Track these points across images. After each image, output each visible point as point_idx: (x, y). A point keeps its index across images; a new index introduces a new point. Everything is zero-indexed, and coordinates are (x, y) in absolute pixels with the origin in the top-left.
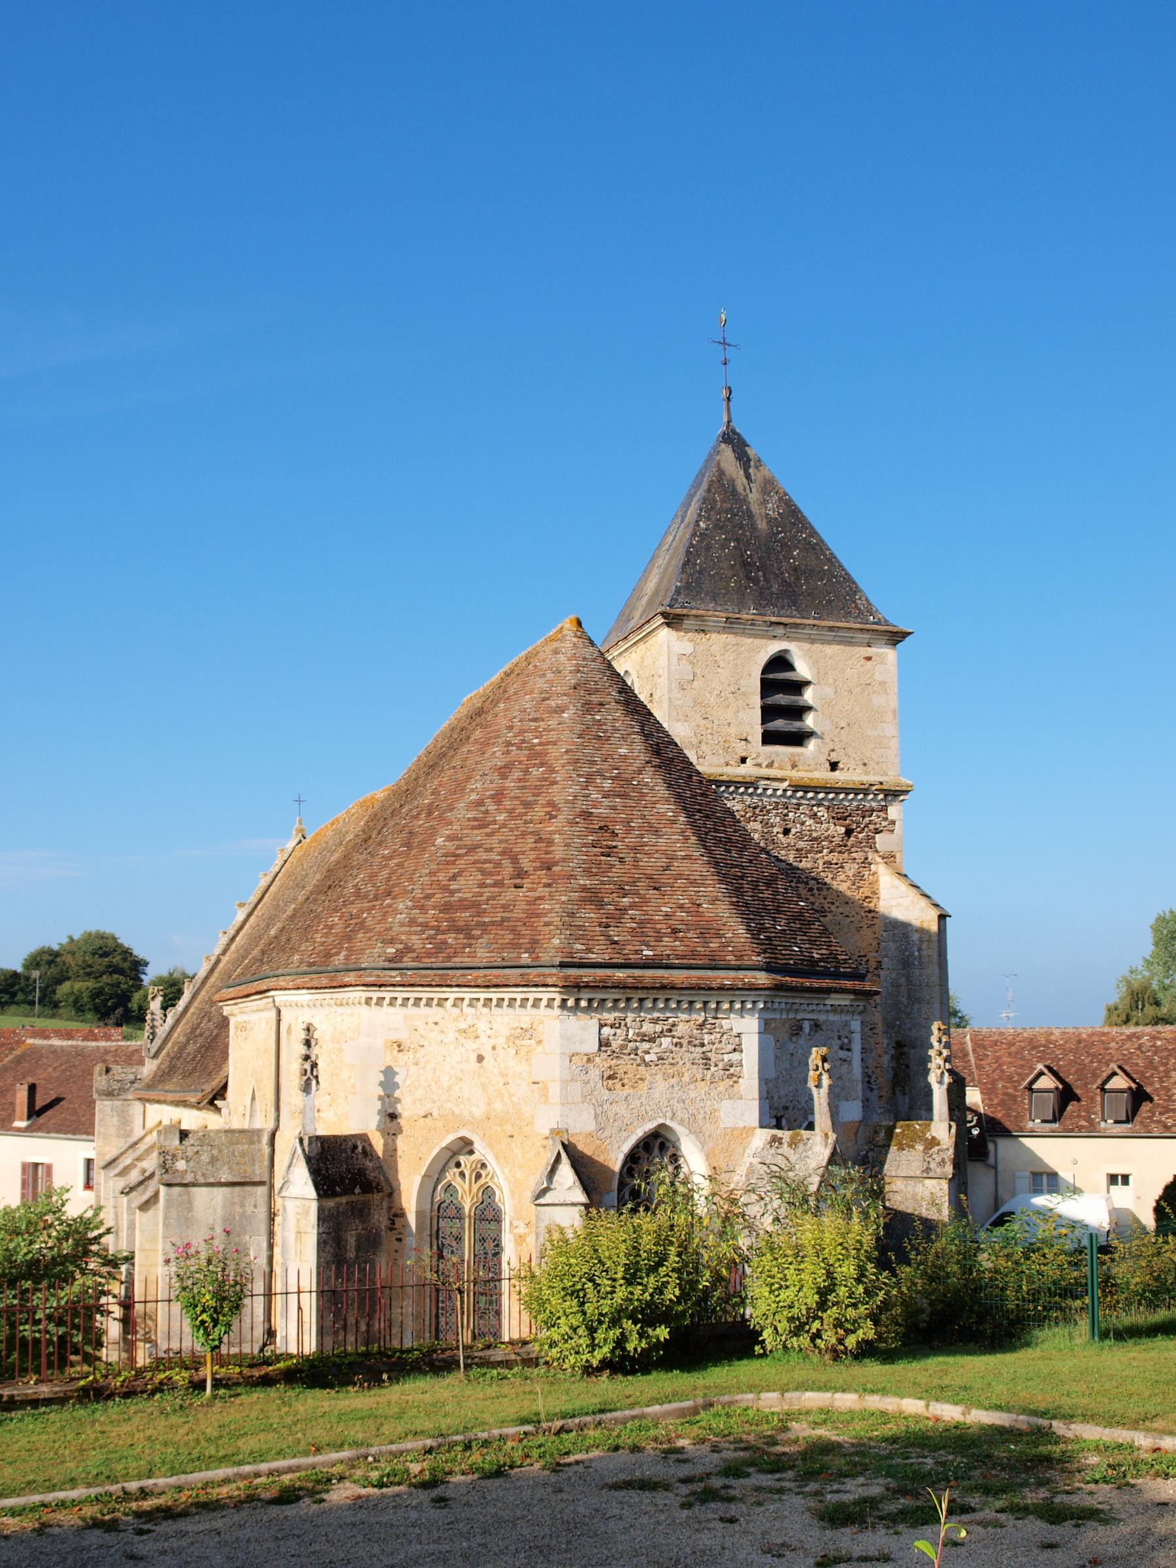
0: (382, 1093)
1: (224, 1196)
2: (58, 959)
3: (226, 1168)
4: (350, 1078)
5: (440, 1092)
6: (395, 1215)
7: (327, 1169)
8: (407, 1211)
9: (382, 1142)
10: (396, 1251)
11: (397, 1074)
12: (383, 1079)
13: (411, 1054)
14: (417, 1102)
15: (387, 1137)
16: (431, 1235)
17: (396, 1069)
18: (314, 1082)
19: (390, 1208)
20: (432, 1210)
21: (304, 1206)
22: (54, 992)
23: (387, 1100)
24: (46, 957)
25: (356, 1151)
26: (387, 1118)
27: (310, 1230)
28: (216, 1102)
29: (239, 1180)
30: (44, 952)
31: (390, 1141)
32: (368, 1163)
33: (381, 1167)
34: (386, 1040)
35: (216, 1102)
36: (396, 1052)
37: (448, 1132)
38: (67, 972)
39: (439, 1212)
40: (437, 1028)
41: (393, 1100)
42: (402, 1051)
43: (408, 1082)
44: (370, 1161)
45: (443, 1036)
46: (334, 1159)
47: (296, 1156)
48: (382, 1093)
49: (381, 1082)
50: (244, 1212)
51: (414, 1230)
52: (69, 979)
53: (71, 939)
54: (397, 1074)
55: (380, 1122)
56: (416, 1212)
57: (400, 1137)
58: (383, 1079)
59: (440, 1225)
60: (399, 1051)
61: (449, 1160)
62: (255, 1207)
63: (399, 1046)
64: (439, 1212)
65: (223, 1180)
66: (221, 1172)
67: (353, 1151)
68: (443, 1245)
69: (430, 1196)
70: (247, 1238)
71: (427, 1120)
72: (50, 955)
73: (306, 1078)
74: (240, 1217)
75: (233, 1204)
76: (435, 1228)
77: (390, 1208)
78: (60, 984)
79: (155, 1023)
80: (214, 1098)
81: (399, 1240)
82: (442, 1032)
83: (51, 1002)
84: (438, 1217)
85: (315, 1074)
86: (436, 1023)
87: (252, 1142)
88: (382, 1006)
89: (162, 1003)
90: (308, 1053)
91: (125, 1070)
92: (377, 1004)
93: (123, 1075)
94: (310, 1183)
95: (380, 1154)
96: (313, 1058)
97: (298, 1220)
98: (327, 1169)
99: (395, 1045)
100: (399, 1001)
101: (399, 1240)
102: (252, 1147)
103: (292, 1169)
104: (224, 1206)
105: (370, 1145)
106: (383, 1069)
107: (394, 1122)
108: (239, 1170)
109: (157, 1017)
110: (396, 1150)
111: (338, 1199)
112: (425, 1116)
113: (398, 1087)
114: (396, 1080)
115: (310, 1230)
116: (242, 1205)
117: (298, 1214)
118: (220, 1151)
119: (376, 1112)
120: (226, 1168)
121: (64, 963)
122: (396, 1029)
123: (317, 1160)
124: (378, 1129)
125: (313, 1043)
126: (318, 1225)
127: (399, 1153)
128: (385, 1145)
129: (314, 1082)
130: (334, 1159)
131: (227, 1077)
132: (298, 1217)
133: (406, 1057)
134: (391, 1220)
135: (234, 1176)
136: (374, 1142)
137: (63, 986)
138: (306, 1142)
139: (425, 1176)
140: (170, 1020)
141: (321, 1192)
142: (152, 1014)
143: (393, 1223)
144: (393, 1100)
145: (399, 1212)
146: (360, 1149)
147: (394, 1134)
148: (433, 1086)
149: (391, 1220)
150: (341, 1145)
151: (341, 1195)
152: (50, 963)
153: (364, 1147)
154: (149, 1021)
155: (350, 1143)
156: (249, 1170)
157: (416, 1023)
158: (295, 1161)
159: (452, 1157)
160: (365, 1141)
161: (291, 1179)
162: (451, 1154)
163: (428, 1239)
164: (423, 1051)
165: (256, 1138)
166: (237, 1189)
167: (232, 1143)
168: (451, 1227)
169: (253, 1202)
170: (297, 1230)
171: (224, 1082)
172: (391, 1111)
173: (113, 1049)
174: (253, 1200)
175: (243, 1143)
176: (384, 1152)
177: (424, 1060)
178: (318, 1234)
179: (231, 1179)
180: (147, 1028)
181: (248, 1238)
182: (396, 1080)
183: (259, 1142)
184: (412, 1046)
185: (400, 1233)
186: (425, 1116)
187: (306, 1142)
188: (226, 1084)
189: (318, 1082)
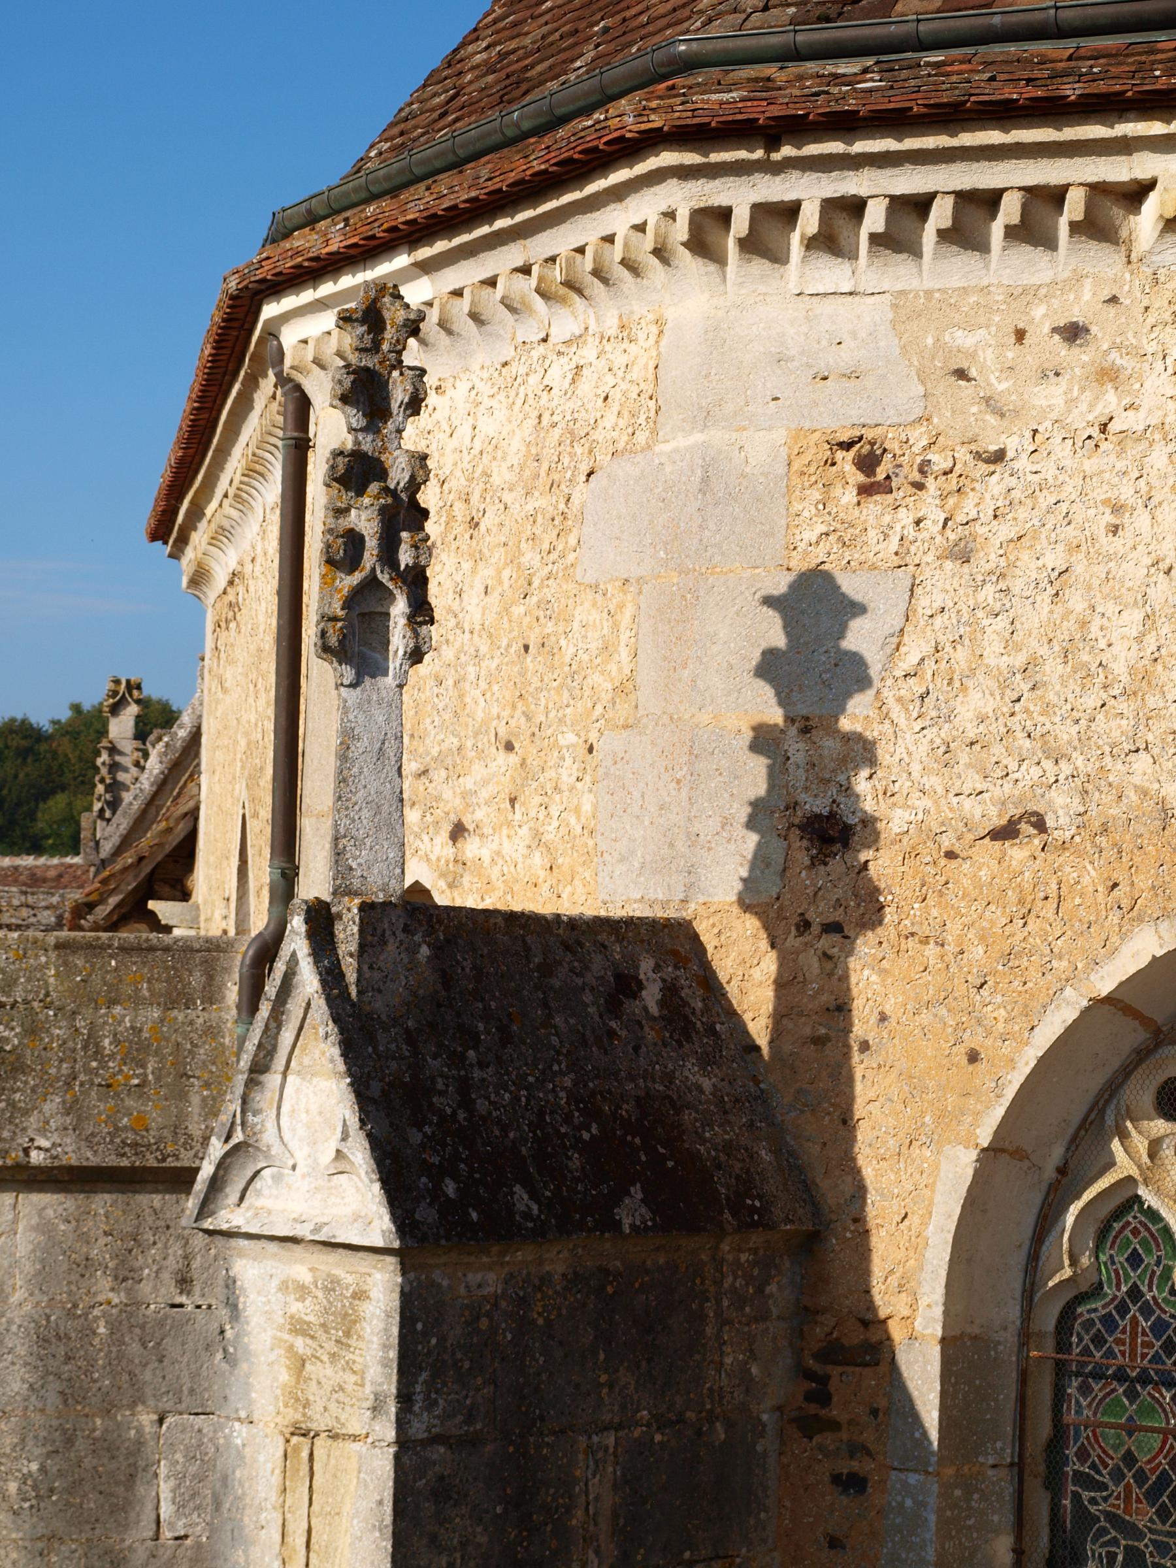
0: (776, 716)
1: (44, 1228)
2: (43, 747)
3: (52, 1105)
4: (607, 649)
5: (1091, 701)
6: (834, 1353)
7: (464, 1087)
8: (897, 1331)
9: (769, 965)
10: (834, 1543)
11: (858, 609)
12: (779, 640)
13: (930, 506)
14: (964, 756)
15: (793, 941)
16: (1019, 1467)
17: (850, 585)
18: (399, 608)
19: (806, 1313)
20: (1026, 1336)
21: (332, 1285)
22: (32, 816)
23: (796, 749)
24: (16, 742)
25: (632, 1007)
26: (799, 845)
27: (357, 1421)
28: (152, 905)
29: (112, 1160)
30: (11, 731)
31: (811, 963)
32: (691, 1072)
33: (762, 1097)
34: (799, 433)
35: (152, 905)
36: (850, 496)
37: (1131, 914)
38: (62, 774)
39: (1062, 1345)
40: (1080, 357)
41: (830, 745)
42: (885, 487)
43: (914, 651)
44: (706, 1062)
45: (1111, 401)
46: (506, 1039)
47: (294, 1008)
48: (776, 716)
49: (770, 655)
50: (135, 1303)
51: (934, 1435)
52: (63, 788)
53: (76, 708)
54: (858, 609)
55: (760, 860)
56: (943, 1340)
57: (866, 946)
58: (779, 640)
59: (1070, 1417)
60: (865, 490)
61: (1126, 1073)
62: (184, 1282)
63: (867, 464)
64: (1062, 1345)
65: (36, 1157)
66: (33, 1121)
67: (613, 1006)
68: (1084, 1518)
69: (1019, 1259)
70: (146, 1419)
71: (1017, 853)
72: (25, 737)
73: (356, 578)
74: (113, 1328)
75: (85, 1267)
76: (1043, 1429)
77: (806, 1313)
78: (45, 800)
79: (122, 776)
80: (150, 888)
81: (854, 1484)
82: (1108, 375)
83: (24, 837)
84: (1061, 1370)
85: (405, 557)
86: (1073, 333)
87: (177, 998)
88: (778, 257)
89: (139, 719)
90: (368, 444)
91: (31, 899)
92: (751, 245)
93: (25, 912)
94: (360, 1155)
95: (759, 1030)
96: (399, 475)
97: (300, 1363)
98: (464, 1087)
99: (846, 459)
100: (875, 219)
101: (854, 1484)
102: (179, 1015)
103: (272, 1080)
104: (41, 1279)
105: (709, 983)
106: (780, 584)
107: (836, 865)
108: (112, 1120)
109: (126, 761)
110: (841, 1009)
111: (521, 1255)
112: (1006, 833)
113: (862, 681)
114: (850, 642)
115: (357, 1421)
116: (125, 1276)
117: (299, 1327)
118: (33, 1030)
119: (743, 813)
120: (52, 1105)
121: (55, 755)
122: (853, 375)
123: (411, 1038)
124: (746, 904)
125: (399, 394)
126: (404, 1398)
127: (862, 1025)
128: (782, 985)
129: (399, 608)
130: (506, 1039)
131: (193, 815)
132: (300, 1344)
133: (905, 518)
134: (809, 1375)
135: (89, 1139)
136: (725, 966)
137: (51, 803)
138: (347, 935)
139: (991, 1155)
140: (155, 765)
141: (426, 1213)
142: (113, 750)
143: (822, 1397)
144: (830, 745)
145: (854, 1336)
146: (651, 996)
147: (834, 928)
148: (1053, 669)
149: (809, 1375)
150: (547, 969)
151: (539, 1234)
152: (24, 754)
153: (670, 991)
154: (104, 771)
155: (598, 963)
156: (156, 1118)
157: (962, 339)
158: (287, 1037)
159: (1141, 1056)
160: (680, 961)
161: (269, 1136)
162: (1133, 1036)
163: (1002, 1483)
164: (997, 483)
165: (196, 979)
166: (102, 1202)
167: (86, 997)
168: (1131, 1429)
169: (173, 1263)
170: (292, 1415)
171: (181, 830)
172: (819, 805)
173: (52, 873)
174: (176, 1250)
175: (137, 1001)
176: (780, 1017)
177: (1005, 530)
178: (404, 1444)
179: (72, 1154)
180: (100, 788)
181: (146, 1419)
182: (850, 642)
183: (212, 996)
184: (940, 462)
185: (857, 1450)
186: (1006, 833)
187: (347, 935)
188: (191, 839)
189: (421, 612)
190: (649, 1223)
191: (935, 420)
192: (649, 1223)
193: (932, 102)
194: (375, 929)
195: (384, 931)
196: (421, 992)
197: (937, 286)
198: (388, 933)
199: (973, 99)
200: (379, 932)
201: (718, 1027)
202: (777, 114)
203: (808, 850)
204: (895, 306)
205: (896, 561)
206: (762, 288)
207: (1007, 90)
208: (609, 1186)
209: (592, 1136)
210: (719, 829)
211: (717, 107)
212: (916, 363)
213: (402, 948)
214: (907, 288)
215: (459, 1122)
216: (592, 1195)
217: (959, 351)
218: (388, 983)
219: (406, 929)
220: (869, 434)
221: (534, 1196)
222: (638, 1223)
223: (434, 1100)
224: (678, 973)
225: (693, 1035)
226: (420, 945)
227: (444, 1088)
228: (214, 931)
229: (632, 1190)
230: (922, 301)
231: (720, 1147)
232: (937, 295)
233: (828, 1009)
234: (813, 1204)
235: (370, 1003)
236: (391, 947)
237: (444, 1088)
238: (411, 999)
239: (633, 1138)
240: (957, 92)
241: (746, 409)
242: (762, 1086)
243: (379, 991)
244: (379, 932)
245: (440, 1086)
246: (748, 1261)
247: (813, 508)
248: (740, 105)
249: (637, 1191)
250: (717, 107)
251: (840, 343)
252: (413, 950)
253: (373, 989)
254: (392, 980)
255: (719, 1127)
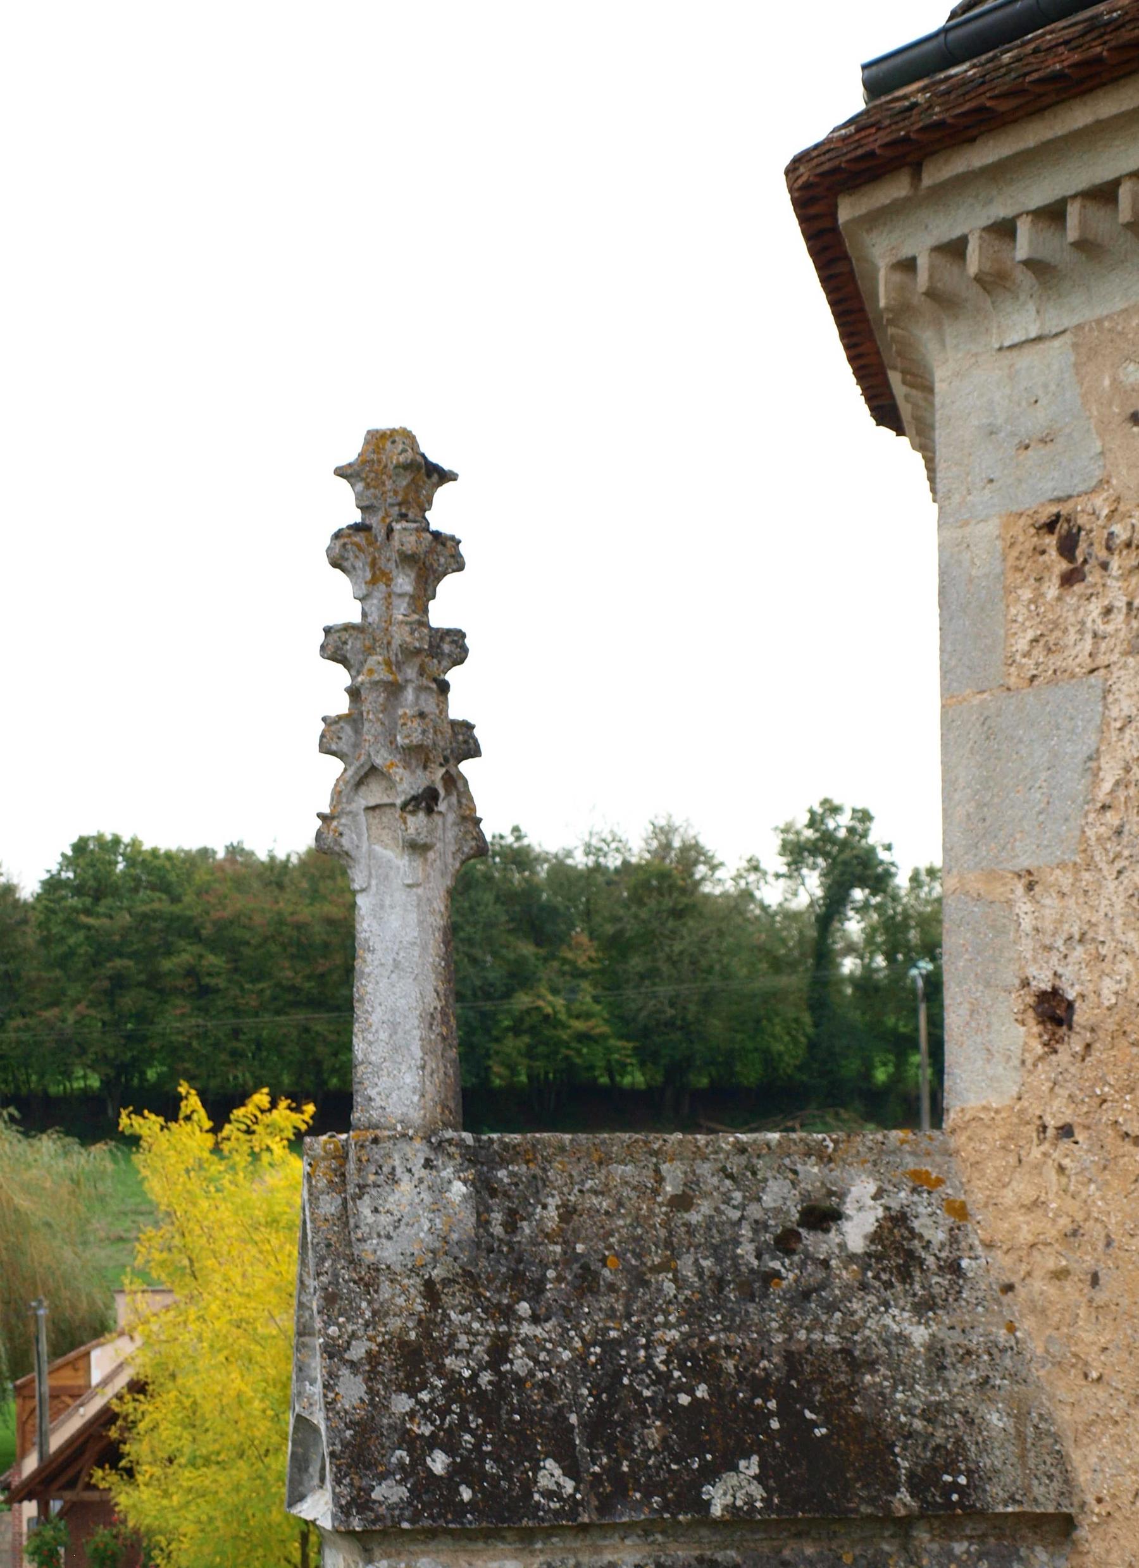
36: (1052, 590)
60: (1069, 579)
123: (431, 1292)
190: (759, 1504)
191: (1114, 481)
192: (759, 1504)
193: (997, 92)
194: (380, 1167)
195: (394, 1168)
196: (455, 1236)
197: (1105, 313)
198: (399, 1171)
199: (1028, 79)
200: (386, 1169)
201: (965, 1263)
202: (888, 139)
203: (1040, 1036)
204: (1075, 346)
205: (1089, 664)
206: (974, 348)
207: (1050, 62)
208: (703, 1459)
209: (695, 1399)
210: (968, 1018)
211: (840, 144)
212: (1095, 413)
213: (423, 1187)
214: (1082, 320)
215: (479, 1387)
216: (670, 1471)
217: (1133, 390)
218: (402, 1228)
219: (428, 1164)
220: (1065, 509)
221: (571, 1472)
222: (739, 1503)
223: (447, 1361)
224: (916, 1198)
225: (917, 1273)
226: (450, 1182)
227: (467, 1346)
228: (267, 1178)
229: (742, 1464)
230: (1096, 333)
231: (918, 1412)
232: (1106, 324)
233: (1066, 1235)
234: (1066, 1481)
235: (375, 1251)
236: (406, 1186)
237: (467, 1346)
238: (437, 1245)
239: (766, 1401)
240: (1013, 75)
241: (969, 498)
242: (1019, 1334)
243: (389, 1237)
244: (386, 1169)
245: (463, 1341)
246: (968, 1552)
247: (1025, 611)
248: (857, 137)
249: (751, 1466)
250: (840, 144)
251: (1036, 402)
252: (439, 1189)
253: (379, 1236)
254: (407, 1224)
255: (925, 1385)
